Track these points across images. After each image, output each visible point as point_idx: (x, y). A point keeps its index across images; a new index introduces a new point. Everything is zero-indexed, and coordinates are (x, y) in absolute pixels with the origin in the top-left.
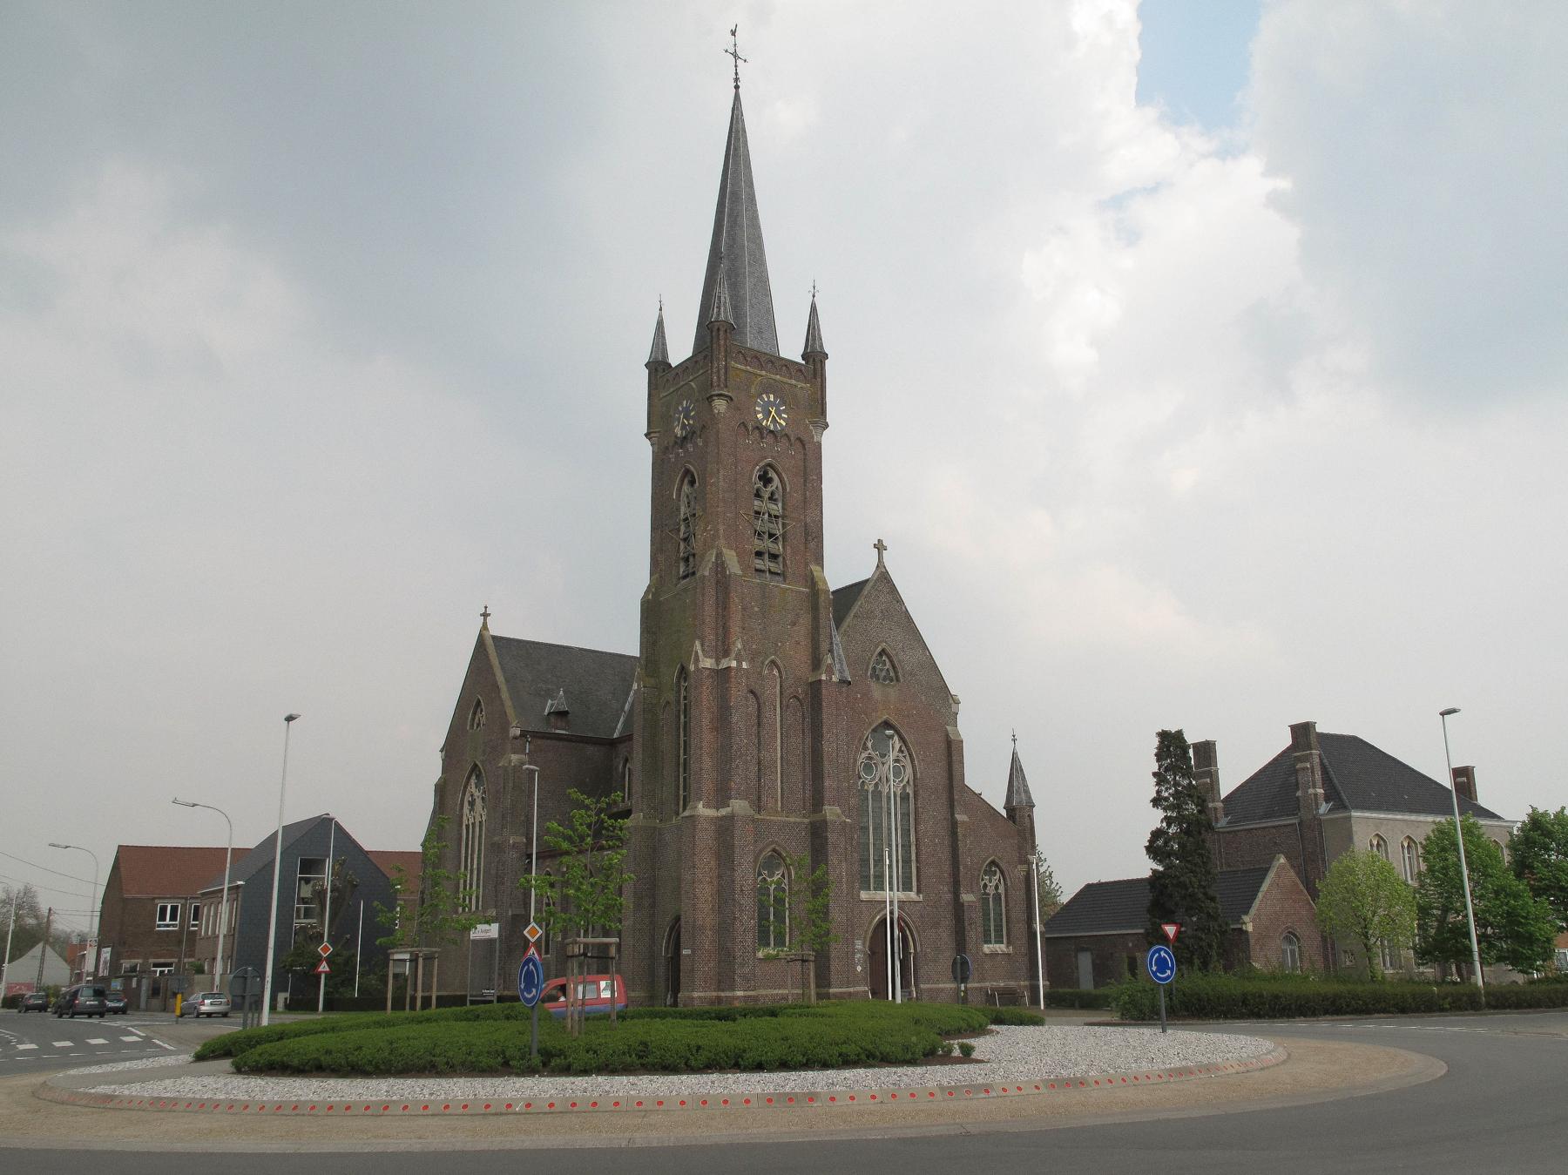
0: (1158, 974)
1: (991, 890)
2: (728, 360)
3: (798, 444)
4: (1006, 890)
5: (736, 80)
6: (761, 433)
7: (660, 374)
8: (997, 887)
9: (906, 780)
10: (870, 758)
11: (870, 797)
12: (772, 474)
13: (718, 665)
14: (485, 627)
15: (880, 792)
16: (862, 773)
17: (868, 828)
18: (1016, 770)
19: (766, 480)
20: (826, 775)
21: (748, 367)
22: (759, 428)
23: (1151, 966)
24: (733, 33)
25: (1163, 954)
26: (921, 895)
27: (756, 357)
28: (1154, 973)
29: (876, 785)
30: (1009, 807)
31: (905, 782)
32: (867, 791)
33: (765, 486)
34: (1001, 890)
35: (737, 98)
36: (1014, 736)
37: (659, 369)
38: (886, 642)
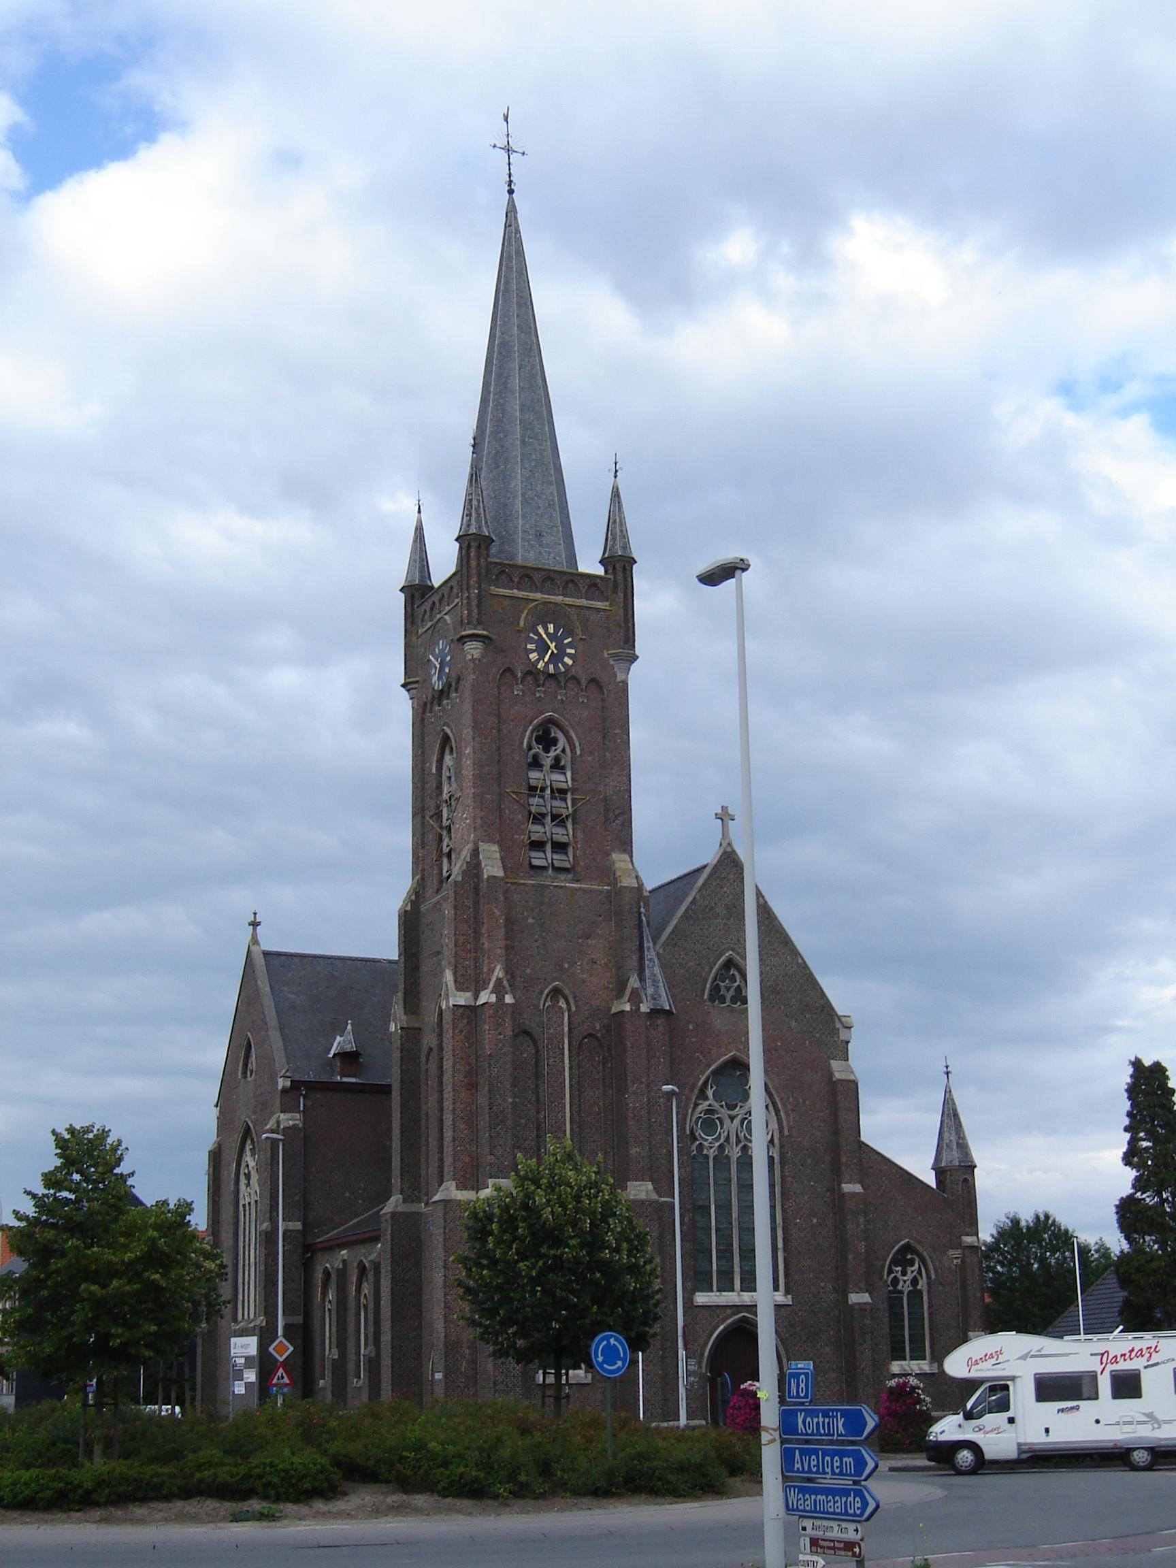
0: (605, 1365)
1: (905, 1287)
2: (483, 586)
3: (593, 687)
4: (929, 1284)
5: (510, 183)
6: (536, 680)
7: (418, 602)
8: (914, 1282)
9: (723, 1136)
10: (710, 1111)
11: (711, 1164)
12: (556, 733)
13: (476, 999)
14: (255, 940)
15: (728, 1157)
16: (699, 1132)
17: (709, 1208)
18: (950, 1116)
19: (547, 741)
20: (631, 1140)
21: (515, 591)
22: (532, 672)
23: (597, 1356)
24: (506, 119)
25: (612, 1341)
26: (789, 1297)
27: (527, 576)
28: (601, 1365)
29: (721, 1147)
30: (939, 1171)
31: (722, 1141)
32: (707, 1157)
33: (547, 751)
34: (922, 1285)
35: (511, 212)
36: (947, 1067)
37: (417, 594)
38: (733, 950)
